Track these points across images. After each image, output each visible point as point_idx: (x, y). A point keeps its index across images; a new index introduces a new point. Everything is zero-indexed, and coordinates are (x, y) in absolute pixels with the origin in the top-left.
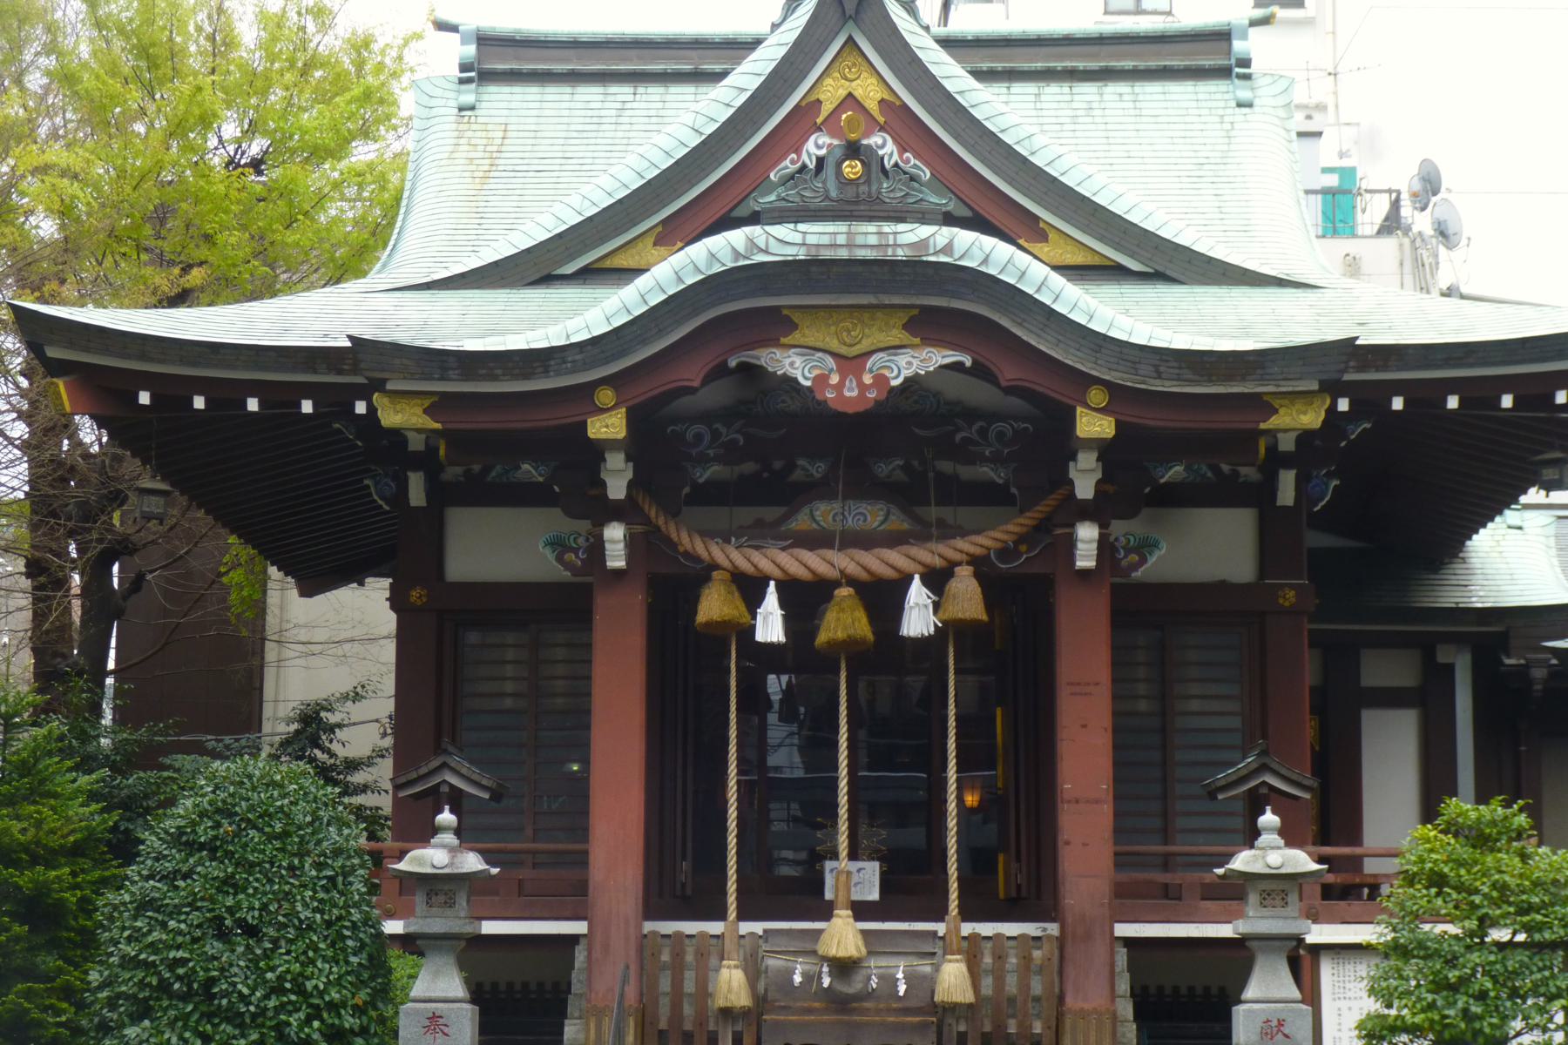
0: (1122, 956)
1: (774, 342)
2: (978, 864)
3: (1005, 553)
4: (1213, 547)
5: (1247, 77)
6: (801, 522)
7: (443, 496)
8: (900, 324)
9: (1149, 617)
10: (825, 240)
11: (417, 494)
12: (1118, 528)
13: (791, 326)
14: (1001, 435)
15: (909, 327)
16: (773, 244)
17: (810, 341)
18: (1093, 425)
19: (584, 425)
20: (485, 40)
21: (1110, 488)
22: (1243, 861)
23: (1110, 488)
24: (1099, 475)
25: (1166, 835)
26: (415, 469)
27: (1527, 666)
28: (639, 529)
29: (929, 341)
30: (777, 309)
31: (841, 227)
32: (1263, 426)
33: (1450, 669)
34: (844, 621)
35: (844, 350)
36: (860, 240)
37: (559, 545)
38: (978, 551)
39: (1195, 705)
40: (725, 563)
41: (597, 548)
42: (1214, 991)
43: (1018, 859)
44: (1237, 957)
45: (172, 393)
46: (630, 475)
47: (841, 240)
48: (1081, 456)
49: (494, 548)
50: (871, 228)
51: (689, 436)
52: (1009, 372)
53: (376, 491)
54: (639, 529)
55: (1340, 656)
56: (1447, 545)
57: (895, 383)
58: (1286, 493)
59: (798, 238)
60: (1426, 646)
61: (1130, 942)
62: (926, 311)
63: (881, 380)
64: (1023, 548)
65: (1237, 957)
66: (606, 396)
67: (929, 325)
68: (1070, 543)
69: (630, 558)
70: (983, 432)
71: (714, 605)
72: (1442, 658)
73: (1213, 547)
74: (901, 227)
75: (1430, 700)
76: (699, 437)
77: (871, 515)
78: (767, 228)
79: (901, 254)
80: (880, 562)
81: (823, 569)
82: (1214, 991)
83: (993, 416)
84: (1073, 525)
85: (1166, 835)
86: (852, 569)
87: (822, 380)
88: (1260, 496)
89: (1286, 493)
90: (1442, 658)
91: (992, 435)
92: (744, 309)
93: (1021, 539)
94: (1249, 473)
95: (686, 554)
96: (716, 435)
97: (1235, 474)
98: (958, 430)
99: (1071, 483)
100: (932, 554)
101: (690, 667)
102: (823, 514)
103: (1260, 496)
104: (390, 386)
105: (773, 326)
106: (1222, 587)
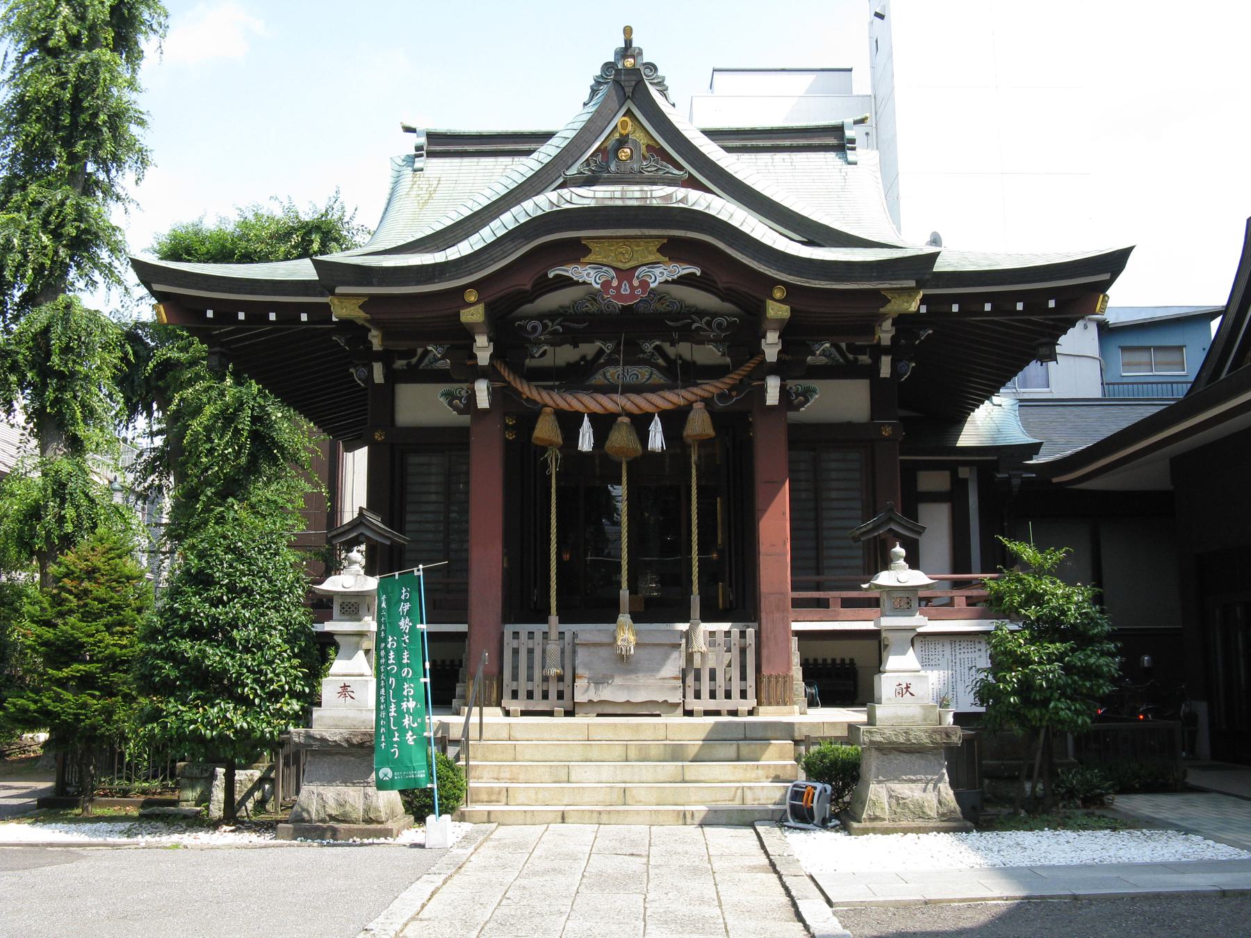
0: (794, 641)
1: (576, 260)
2: (710, 576)
3: (722, 396)
4: (843, 401)
5: (854, 149)
6: (598, 379)
7: (393, 377)
8: (655, 249)
9: (811, 441)
10: (608, 195)
11: (378, 377)
12: (791, 384)
13: (587, 251)
14: (720, 325)
15: (661, 250)
16: (575, 199)
17: (600, 260)
18: (777, 310)
19: (458, 315)
20: (432, 137)
21: (787, 358)
22: (885, 578)
23: (787, 358)
24: (779, 347)
25: (818, 571)
26: (377, 361)
27: (1009, 478)
28: (498, 384)
29: (674, 259)
30: (578, 240)
31: (618, 188)
32: (882, 310)
33: (965, 481)
34: (621, 438)
35: (620, 265)
36: (629, 195)
37: (450, 396)
38: (706, 394)
39: (834, 495)
40: (551, 403)
41: (472, 397)
42: (847, 661)
43: (731, 586)
44: (876, 642)
45: (226, 311)
46: (491, 350)
47: (618, 195)
48: (768, 335)
49: (421, 405)
50: (637, 188)
51: (529, 328)
52: (722, 280)
53: (357, 374)
54: (498, 384)
55: (909, 473)
56: (959, 419)
57: (652, 286)
58: (885, 371)
59: (591, 194)
60: (952, 468)
61: (799, 634)
62: (672, 240)
63: (644, 284)
64: (734, 393)
65: (876, 642)
66: (471, 297)
67: (674, 250)
68: (763, 390)
69: (492, 402)
70: (709, 324)
71: (546, 430)
72: (961, 475)
73: (843, 401)
74: (654, 187)
75: (955, 497)
76: (535, 328)
77: (642, 374)
78: (573, 189)
79: (655, 203)
80: (642, 403)
81: (611, 407)
82: (847, 661)
83: (714, 315)
84: (764, 379)
85: (818, 571)
86: (629, 406)
87: (606, 285)
88: (871, 372)
89: (885, 371)
90: (961, 475)
91: (714, 325)
92: (558, 239)
93: (732, 388)
94: (865, 359)
95: (528, 399)
96: (545, 327)
97: (856, 360)
98: (694, 322)
99: (763, 353)
100: (672, 399)
101: (522, 459)
102: (613, 373)
103: (871, 372)
104: (339, 290)
105: (576, 251)
106: (850, 425)
